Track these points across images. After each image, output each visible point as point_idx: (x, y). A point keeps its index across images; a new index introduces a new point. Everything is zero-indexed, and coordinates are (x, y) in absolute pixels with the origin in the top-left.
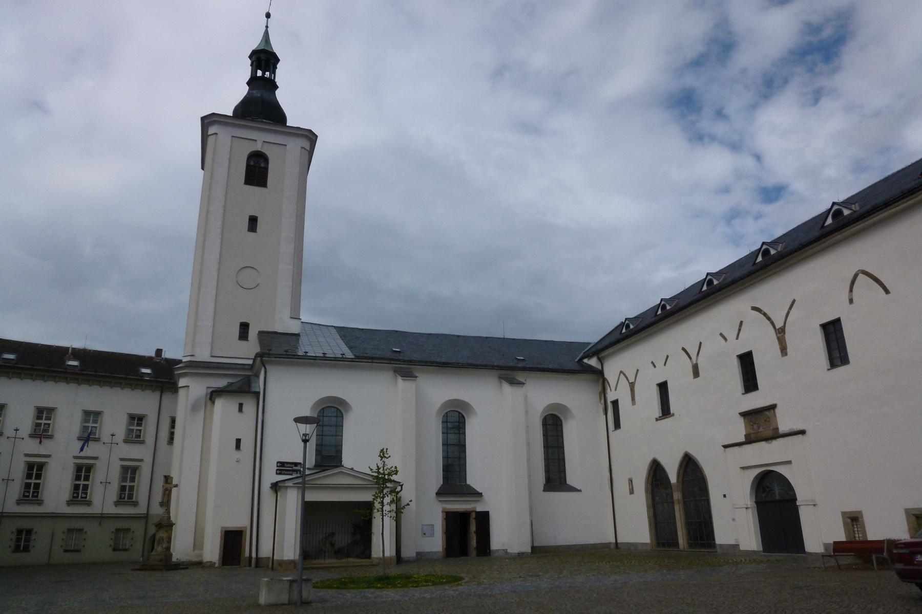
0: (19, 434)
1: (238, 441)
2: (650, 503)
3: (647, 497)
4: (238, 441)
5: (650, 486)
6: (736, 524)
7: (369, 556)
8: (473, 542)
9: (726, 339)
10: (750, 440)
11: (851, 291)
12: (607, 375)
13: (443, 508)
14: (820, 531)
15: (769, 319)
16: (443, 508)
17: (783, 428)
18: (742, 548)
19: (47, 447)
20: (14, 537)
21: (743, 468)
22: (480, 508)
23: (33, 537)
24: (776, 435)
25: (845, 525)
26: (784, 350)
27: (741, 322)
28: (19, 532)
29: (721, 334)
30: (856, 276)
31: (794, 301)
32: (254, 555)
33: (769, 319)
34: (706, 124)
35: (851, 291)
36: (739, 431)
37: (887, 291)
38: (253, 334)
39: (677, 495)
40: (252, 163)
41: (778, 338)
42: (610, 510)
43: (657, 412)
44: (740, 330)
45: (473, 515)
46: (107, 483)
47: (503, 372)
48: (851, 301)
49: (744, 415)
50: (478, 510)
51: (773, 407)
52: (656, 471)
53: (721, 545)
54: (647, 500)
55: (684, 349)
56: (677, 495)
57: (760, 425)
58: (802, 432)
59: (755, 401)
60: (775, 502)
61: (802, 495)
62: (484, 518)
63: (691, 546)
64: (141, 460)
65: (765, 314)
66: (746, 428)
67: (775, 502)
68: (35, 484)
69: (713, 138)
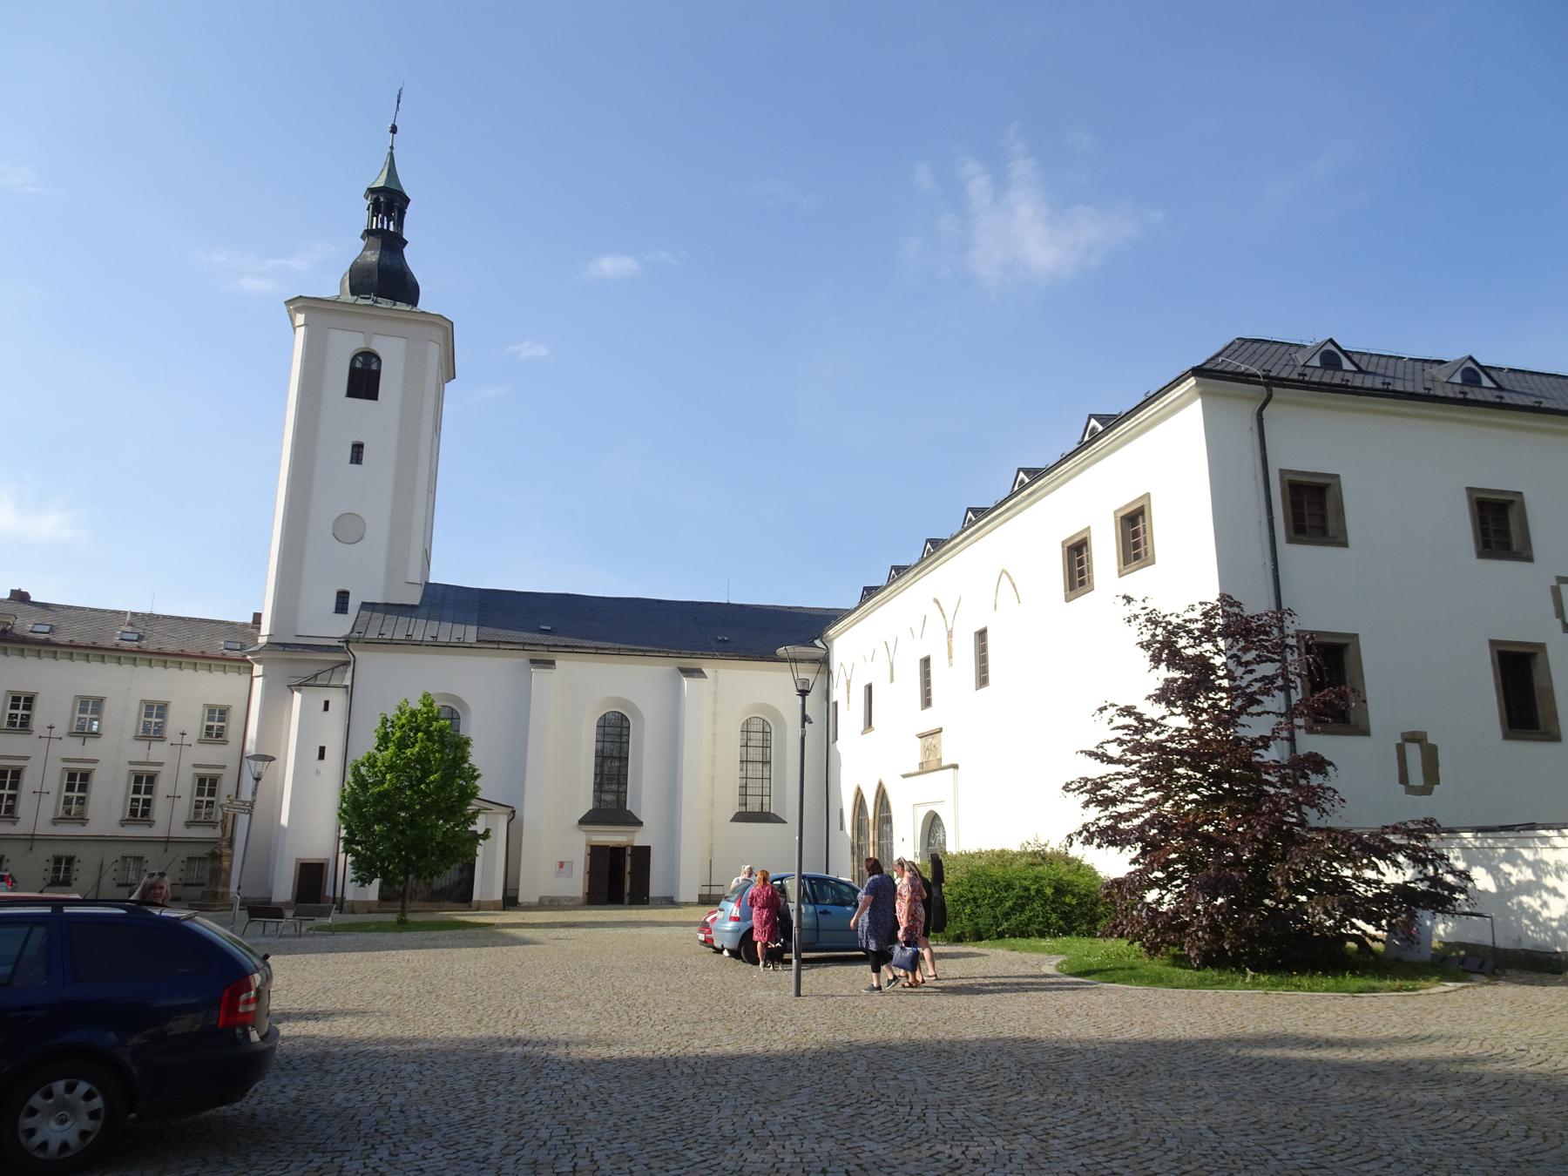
0: (55, 733)
1: (322, 750)
4: (322, 750)
19: (91, 749)
20: (51, 866)
22: (639, 838)
23: (76, 866)
28: (58, 860)
32: (339, 895)
38: (354, 603)
40: (358, 365)
45: (629, 851)
46: (173, 797)
50: (636, 844)
59: (928, 720)
64: (224, 767)
68: (79, 798)
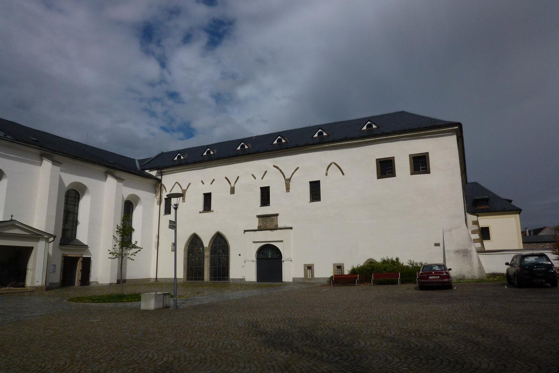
2: (186, 257)
3: (184, 253)
5: (187, 248)
6: (243, 267)
7: (24, 286)
8: (78, 276)
9: (255, 178)
10: (260, 229)
11: (327, 170)
12: (163, 182)
13: (63, 254)
14: (291, 271)
15: (282, 173)
16: (63, 254)
17: (280, 225)
18: (246, 280)
21: (254, 242)
24: (276, 228)
25: (305, 270)
26: (288, 189)
27: (266, 172)
29: (252, 175)
30: (331, 164)
31: (298, 168)
33: (282, 173)
34: (152, 46)
35: (327, 170)
36: (255, 224)
37: (343, 174)
39: (207, 253)
41: (286, 183)
42: (159, 259)
43: (202, 209)
44: (264, 175)
45: (81, 259)
47: (109, 169)
48: (327, 174)
49: (259, 217)
51: (277, 215)
52: (195, 240)
53: (233, 279)
54: (184, 255)
55: (226, 178)
56: (207, 253)
57: (268, 222)
58: (291, 228)
59: (266, 211)
60: (269, 260)
61: (284, 258)
62: (87, 262)
63: (211, 279)
65: (280, 171)
66: (259, 223)
67: (269, 260)
69: (153, 54)
